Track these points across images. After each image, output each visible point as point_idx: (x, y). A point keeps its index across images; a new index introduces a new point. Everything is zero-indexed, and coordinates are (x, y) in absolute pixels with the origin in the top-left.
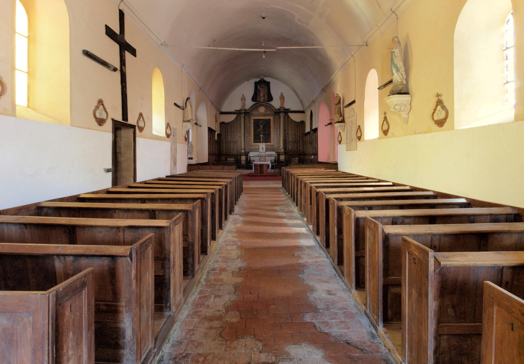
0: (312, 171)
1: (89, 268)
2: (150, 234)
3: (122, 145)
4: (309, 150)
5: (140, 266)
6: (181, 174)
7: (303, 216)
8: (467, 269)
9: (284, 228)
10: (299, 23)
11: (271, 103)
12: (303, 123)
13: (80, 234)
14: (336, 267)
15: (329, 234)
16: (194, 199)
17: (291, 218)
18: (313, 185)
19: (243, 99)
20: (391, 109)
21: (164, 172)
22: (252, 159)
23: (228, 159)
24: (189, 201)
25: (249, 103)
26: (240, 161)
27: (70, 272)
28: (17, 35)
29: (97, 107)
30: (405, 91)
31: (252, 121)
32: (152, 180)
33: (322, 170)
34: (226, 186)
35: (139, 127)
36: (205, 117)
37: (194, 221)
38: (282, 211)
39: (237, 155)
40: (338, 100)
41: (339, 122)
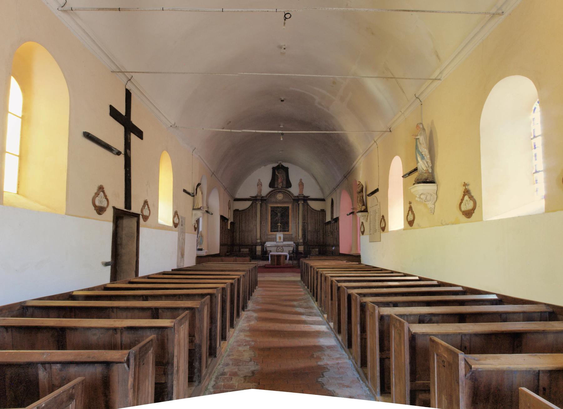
0: (333, 263)
1: (79, 377)
2: (152, 336)
3: (124, 236)
4: (330, 240)
5: (139, 372)
6: (189, 267)
7: (323, 312)
8: (501, 373)
9: (302, 325)
10: (320, 107)
11: (290, 189)
12: (323, 211)
13: (71, 337)
14: (359, 369)
15: (351, 335)
16: (203, 296)
17: (310, 314)
18: (334, 279)
19: (260, 184)
20: (417, 199)
21: (169, 265)
22: (268, 249)
23: (242, 250)
24: (197, 297)
25: (266, 190)
26: (256, 251)
27: (56, 383)
28: (9, 115)
29: (97, 194)
30: (431, 179)
31: (269, 209)
32: (156, 274)
33: (344, 263)
34: (239, 280)
35: (143, 215)
36: (217, 205)
37: (202, 320)
38: (300, 306)
39: (252, 246)
40: (360, 188)
41: (361, 211)
